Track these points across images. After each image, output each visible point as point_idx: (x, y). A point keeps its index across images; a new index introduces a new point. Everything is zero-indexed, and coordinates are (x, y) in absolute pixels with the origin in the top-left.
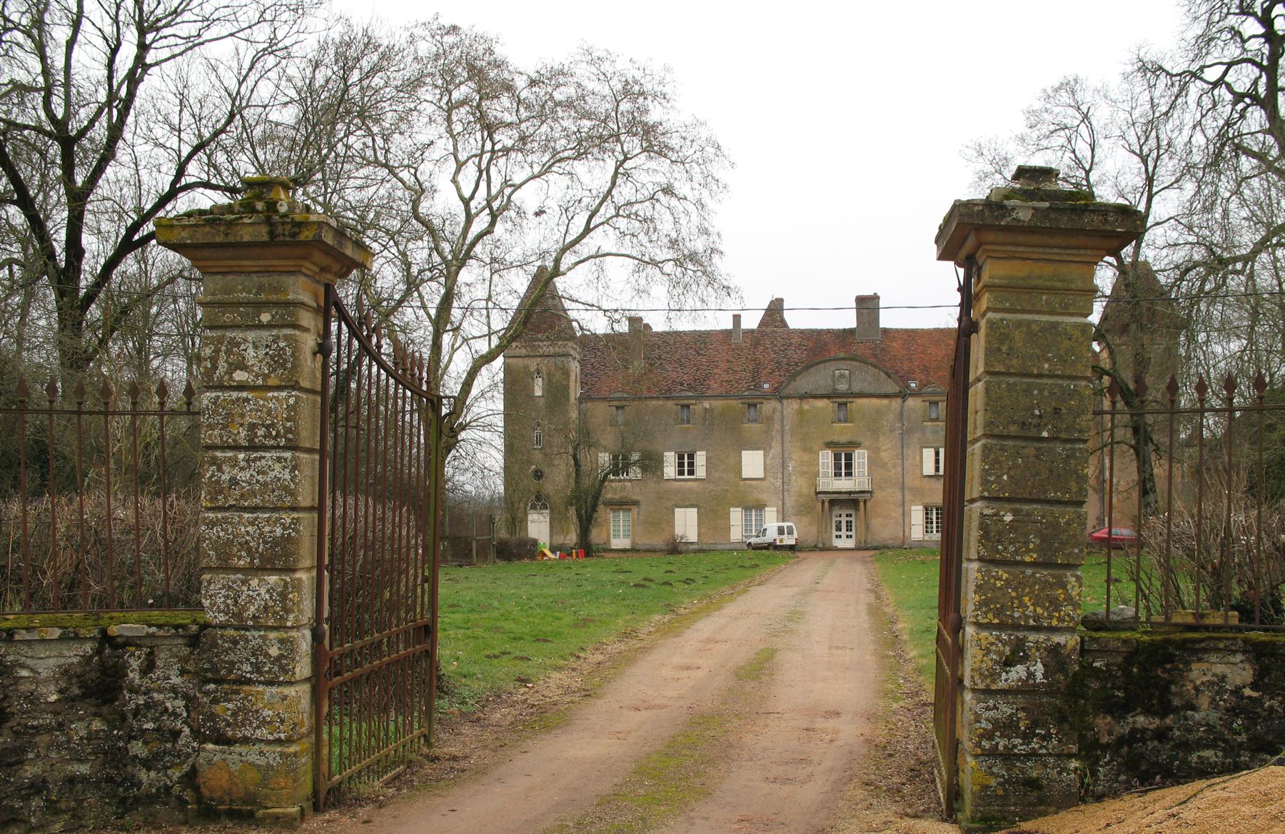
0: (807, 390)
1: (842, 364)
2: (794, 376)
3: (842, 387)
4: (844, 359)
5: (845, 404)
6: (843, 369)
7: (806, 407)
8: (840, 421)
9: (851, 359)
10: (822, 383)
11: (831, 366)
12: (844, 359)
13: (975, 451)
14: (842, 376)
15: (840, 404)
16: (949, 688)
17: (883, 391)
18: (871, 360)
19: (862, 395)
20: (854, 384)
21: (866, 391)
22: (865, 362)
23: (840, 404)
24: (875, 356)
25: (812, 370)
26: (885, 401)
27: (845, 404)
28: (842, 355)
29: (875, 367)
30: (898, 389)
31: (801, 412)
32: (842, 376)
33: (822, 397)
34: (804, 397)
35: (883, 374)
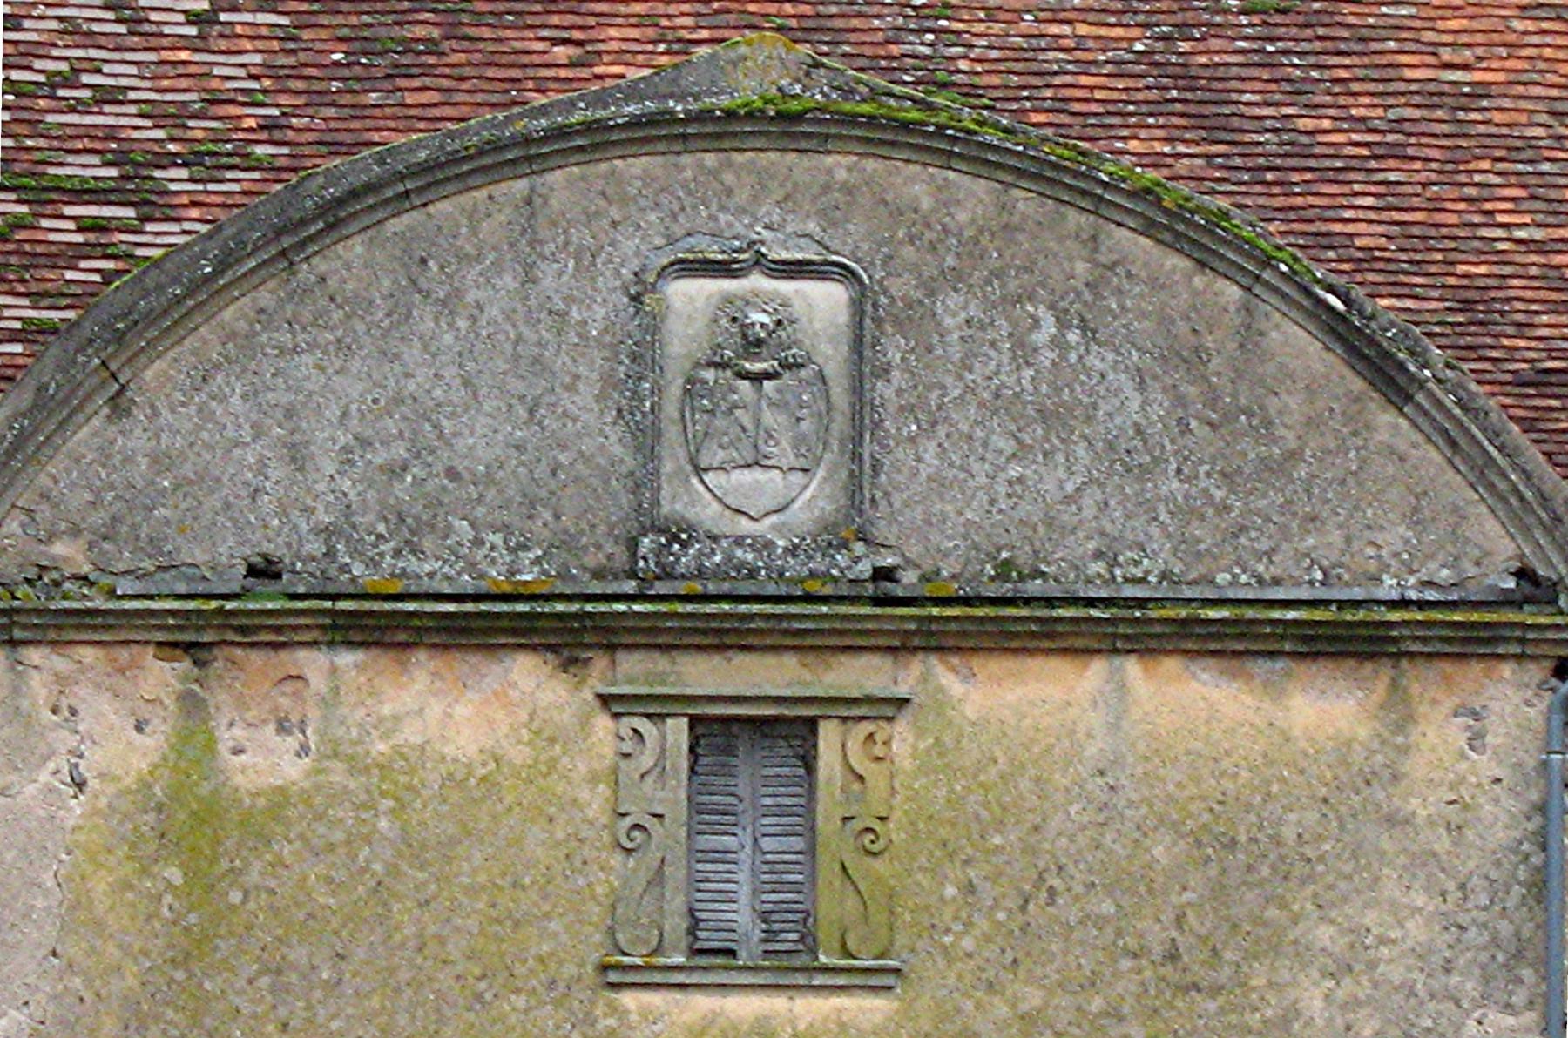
0: (294, 540)
1: (769, 197)
2: (114, 335)
3: (758, 499)
4: (785, 125)
5: (790, 731)
6: (777, 260)
7: (260, 761)
8: (711, 956)
9: (885, 134)
10: (480, 438)
11: (625, 210)
12: (785, 125)
13: (451, 607)
14: (754, 352)
15: (718, 733)
16: (62, 425)
17: (1299, 561)
18: (1131, 153)
19: (1011, 617)
20: (913, 463)
21: (1073, 563)
22: (1065, 179)
23: (718, 733)
24: (1196, 100)
25: (351, 259)
26: (1324, 710)
27: (790, 731)
28: (759, 68)
29: (1196, 237)
30: (1491, 549)
31: (189, 825)
32: (754, 352)
33: (474, 626)
34: (222, 624)
35: (1296, 344)
